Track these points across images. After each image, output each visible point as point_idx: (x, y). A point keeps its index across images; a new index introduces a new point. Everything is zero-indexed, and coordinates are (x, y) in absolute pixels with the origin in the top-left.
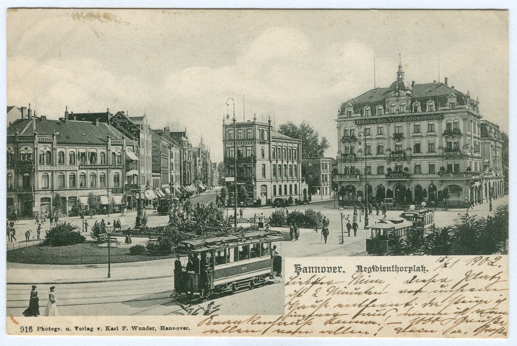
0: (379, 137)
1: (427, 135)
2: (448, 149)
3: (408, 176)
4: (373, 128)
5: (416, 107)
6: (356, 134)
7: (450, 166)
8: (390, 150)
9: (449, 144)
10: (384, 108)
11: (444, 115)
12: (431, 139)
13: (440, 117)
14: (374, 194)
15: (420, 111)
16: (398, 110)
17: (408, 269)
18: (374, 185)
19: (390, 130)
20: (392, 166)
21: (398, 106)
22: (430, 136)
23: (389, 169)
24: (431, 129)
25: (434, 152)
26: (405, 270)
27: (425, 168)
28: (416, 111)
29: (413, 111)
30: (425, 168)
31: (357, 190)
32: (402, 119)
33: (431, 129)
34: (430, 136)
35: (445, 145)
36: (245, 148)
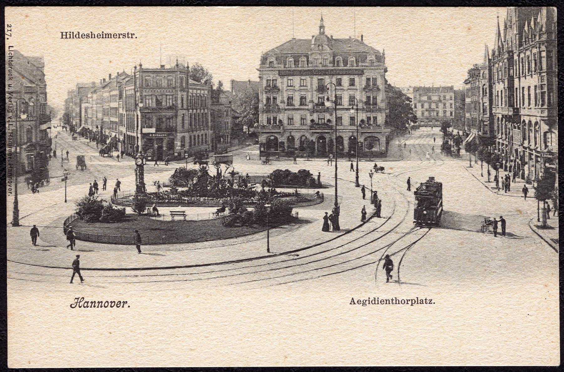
0: (295, 87)
1: (300, 90)
2: (367, 103)
3: (331, 128)
4: (296, 80)
5: (338, 61)
6: (279, 84)
7: (369, 118)
8: (312, 102)
9: (368, 98)
10: (308, 61)
11: (365, 71)
12: (352, 92)
13: (361, 73)
14: (297, 144)
15: (342, 65)
16: (321, 63)
17: (410, 303)
18: (297, 136)
19: (313, 82)
20: (315, 117)
21: (320, 59)
22: (351, 91)
23: (312, 121)
24: (352, 83)
25: (341, 105)
26: (407, 303)
27: (346, 120)
28: (338, 65)
29: (336, 65)
30: (346, 120)
31: (280, 141)
32: (325, 73)
33: (352, 83)
34: (351, 91)
35: (364, 100)
36: (165, 96)
